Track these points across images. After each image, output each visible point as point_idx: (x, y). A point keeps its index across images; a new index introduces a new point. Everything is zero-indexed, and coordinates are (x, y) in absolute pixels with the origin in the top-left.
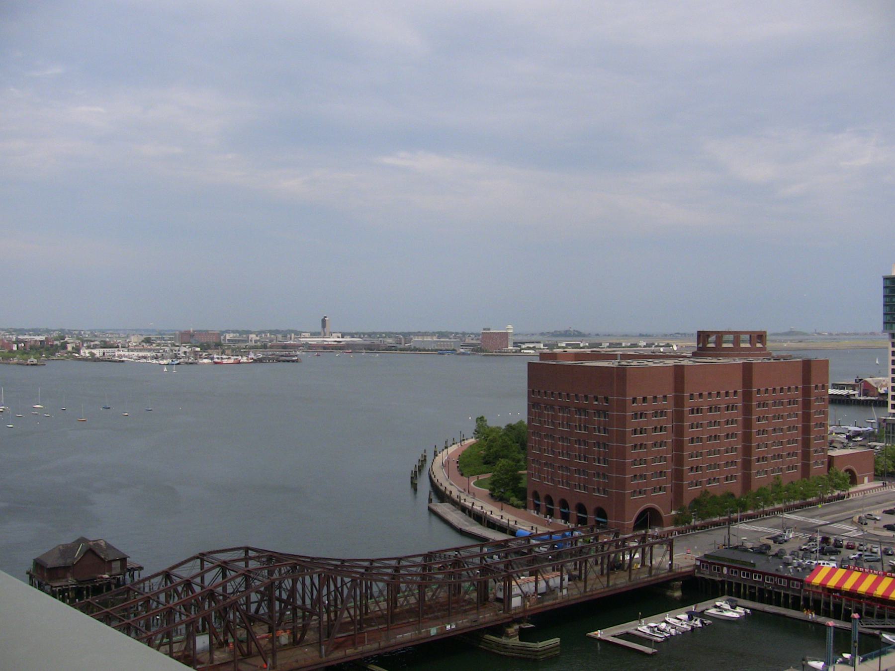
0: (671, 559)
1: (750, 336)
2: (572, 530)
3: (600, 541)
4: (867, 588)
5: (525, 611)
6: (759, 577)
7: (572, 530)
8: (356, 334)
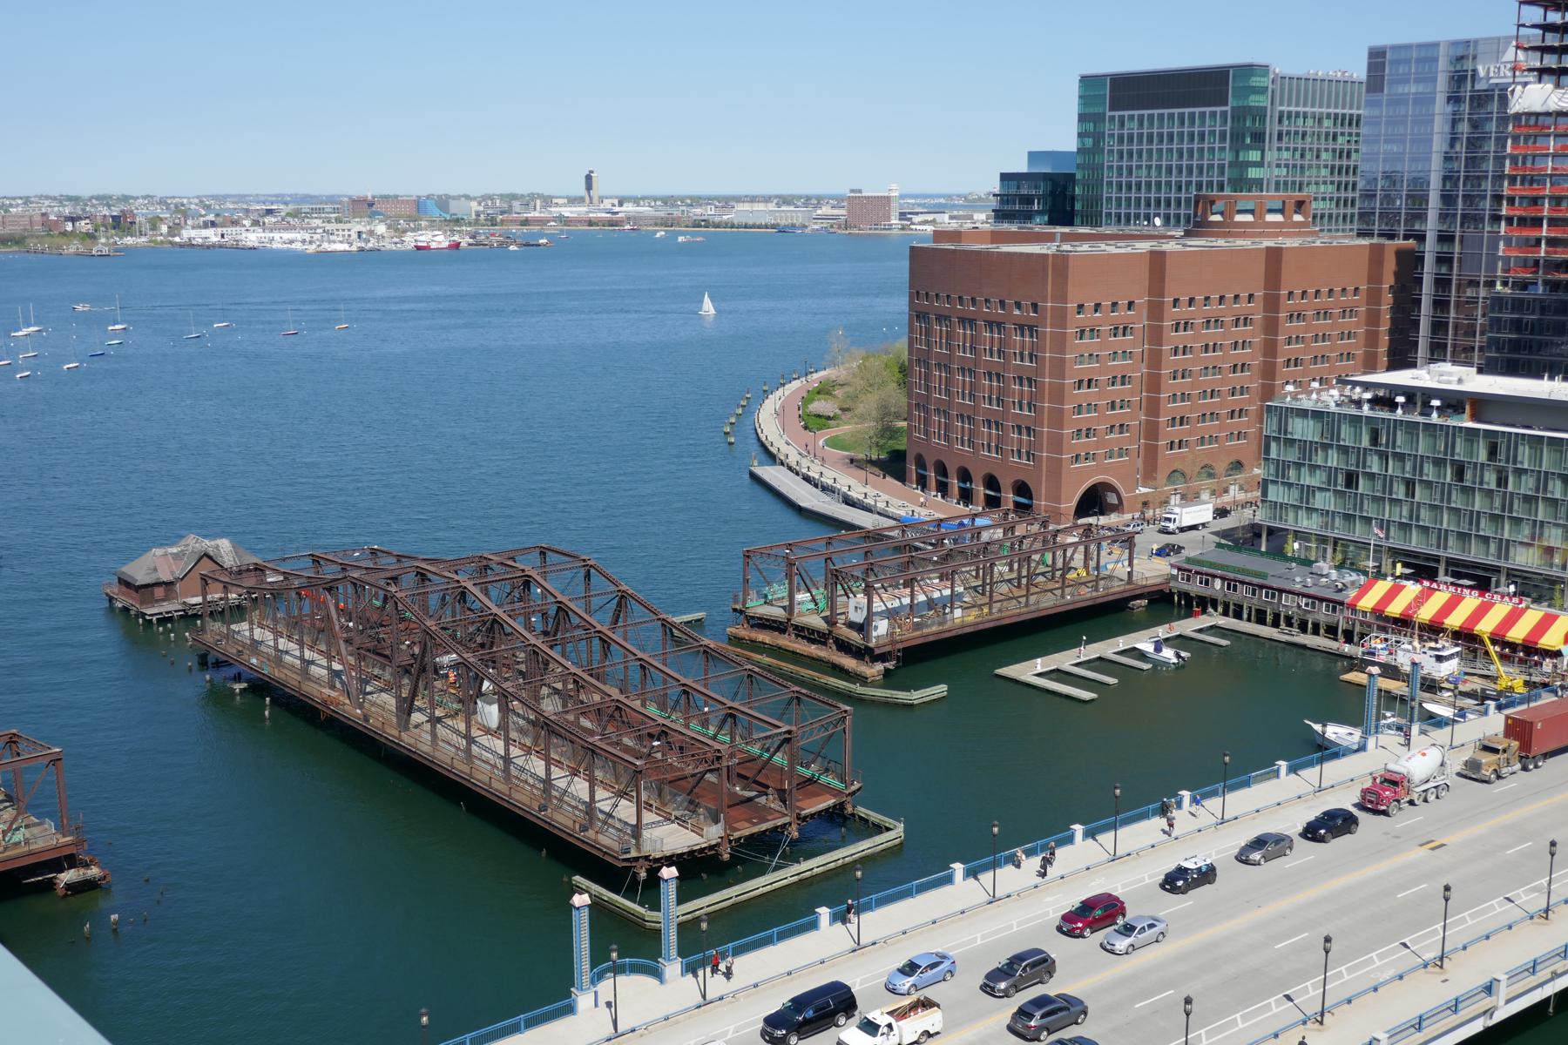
0: (1131, 564)
1: (1284, 202)
2: (974, 517)
3: (1017, 534)
4: (1434, 612)
5: (893, 642)
6: (1273, 596)
7: (974, 517)
8: (644, 198)
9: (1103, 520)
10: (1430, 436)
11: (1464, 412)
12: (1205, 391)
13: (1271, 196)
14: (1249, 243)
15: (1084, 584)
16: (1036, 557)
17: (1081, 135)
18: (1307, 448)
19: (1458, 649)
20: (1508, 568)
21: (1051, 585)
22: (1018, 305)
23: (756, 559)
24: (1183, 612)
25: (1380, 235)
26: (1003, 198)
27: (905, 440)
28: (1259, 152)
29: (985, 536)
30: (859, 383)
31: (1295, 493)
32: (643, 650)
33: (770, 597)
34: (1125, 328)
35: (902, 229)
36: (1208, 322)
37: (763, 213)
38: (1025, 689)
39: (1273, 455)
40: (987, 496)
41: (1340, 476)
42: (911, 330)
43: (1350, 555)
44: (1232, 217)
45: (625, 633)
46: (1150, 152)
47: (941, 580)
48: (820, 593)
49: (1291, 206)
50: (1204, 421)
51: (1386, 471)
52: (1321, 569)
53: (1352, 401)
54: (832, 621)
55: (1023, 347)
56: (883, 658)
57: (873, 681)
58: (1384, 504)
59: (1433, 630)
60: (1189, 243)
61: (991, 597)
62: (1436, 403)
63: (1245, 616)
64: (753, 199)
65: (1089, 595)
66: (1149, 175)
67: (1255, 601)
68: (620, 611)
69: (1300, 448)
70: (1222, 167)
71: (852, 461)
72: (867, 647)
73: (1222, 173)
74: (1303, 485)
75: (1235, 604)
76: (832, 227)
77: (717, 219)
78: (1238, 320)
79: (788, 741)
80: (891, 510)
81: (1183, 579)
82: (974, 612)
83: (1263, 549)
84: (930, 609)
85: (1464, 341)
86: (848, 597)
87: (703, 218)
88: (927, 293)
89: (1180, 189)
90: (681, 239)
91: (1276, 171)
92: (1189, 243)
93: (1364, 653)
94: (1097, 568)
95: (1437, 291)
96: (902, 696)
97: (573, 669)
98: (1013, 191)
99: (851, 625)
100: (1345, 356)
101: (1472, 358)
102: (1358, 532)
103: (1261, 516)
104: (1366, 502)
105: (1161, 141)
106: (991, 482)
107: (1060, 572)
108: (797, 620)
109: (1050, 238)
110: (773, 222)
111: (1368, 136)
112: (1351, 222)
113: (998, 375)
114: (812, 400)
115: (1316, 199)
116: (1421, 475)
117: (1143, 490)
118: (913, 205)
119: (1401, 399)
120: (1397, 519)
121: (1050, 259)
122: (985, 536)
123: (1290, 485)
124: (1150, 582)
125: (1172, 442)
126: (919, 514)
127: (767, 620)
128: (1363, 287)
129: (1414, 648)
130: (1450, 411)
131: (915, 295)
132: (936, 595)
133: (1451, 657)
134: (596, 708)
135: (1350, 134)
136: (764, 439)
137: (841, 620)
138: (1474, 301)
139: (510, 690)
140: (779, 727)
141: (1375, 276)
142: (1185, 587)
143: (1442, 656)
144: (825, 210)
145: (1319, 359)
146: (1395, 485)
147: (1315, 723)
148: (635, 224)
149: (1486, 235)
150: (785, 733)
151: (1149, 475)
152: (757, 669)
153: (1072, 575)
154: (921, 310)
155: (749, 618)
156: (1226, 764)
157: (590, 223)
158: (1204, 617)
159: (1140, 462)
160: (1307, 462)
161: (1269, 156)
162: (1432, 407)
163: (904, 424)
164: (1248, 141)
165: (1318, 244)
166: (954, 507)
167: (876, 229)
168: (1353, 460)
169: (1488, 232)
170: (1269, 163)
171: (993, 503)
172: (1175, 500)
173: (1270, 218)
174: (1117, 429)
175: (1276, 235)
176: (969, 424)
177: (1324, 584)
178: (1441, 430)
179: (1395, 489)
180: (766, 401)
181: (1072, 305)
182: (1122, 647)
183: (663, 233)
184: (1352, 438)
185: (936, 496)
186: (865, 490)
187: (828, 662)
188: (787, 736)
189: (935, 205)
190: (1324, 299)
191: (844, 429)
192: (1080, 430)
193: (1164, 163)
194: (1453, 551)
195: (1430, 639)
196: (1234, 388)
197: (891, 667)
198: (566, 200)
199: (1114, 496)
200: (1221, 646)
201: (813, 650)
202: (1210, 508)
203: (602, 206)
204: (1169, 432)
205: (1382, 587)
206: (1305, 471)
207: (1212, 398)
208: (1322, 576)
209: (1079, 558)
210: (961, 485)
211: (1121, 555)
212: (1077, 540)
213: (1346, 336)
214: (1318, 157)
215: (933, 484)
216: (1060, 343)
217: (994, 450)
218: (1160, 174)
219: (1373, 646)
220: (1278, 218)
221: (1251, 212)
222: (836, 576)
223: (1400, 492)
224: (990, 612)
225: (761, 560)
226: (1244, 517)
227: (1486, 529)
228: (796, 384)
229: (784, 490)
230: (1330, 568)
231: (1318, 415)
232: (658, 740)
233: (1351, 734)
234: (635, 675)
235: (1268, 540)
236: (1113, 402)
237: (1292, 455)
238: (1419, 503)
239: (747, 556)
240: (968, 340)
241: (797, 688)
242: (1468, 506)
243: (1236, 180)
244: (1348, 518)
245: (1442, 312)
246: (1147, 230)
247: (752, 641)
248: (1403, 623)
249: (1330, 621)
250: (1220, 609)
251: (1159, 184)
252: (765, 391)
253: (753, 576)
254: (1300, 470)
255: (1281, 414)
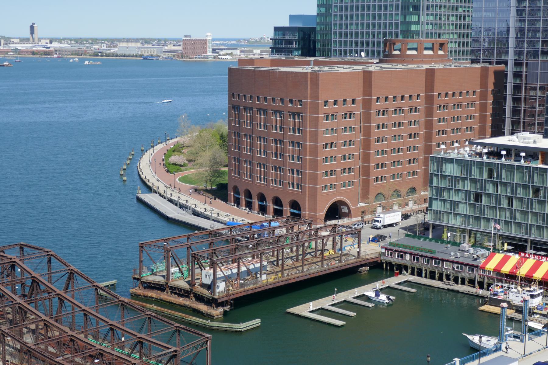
1: (433, 44)
3: (295, 231)
4: (544, 274)
5: (228, 295)
8: (64, 39)
9: (341, 222)
10: (520, 172)
11: (538, 159)
12: (394, 149)
13: (427, 41)
14: (416, 66)
15: (333, 258)
16: (306, 244)
17: (319, 6)
18: (453, 180)
19: (542, 291)
20: (531, 240)
21: (315, 260)
22: (291, 101)
23: (147, 248)
24: (388, 273)
25: (483, 62)
26: (275, 40)
27: (227, 178)
28: (417, 16)
29: (277, 232)
30: (198, 145)
31: (448, 205)
32: (86, 305)
33: (155, 270)
34: (350, 114)
35: (214, 58)
36: (396, 110)
37: (133, 48)
38: (297, 318)
39: (435, 184)
40: (275, 210)
41: (472, 196)
42: (230, 115)
43: (478, 239)
44: (405, 52)
45: (73, 295)
46: (357, 16)
47: (253, 258)
48: (184, 267)
49: (437, 46)
50: (394, 166)
51: (497, 192)
52: (465, 247)
53: (477, 154)
54: (191, 283)
55: (294, 125)
56: (223, 304)
57: (217, 318)
58: (528, 216)
59: (528, 280)
60: (383, 66)
61: (283, 267)
62: (523, 154)
63: (424, 275)
64: (128, 40)
65: (337, 265)
66: (357, 29)
67: (429, 266)
68: (69, 282)
69: (449, 180)
70: (397, 24)
71: (196, 190)
72: (213, 299)
73: (397, 27)
74: (451, 201)
75: (417, 269)
76: (174, 56)
77: (108, 52)
78: (411, 109)
79: (175, 356)
80: (221, 218)
81: (388, 255)
82: (273, 276)
83: (430, 237)
84: (248, 275)
85: (529, 120)
86: (202, 270)
87: (99, 51)
88: (239, 95)
89: (374, 36)
90: (86, 62)
91: (426, 27)
92: (383, 66)
93: (491, 295)
94: (341, 249)
95: (514, 93)
96: (235, 326)
97: (44, 317)
98: (281, 37)
99: (203, 286)
100: (469, 129)
101: (534, 129)
102: (483, 227)
103: (429, 218)
104: (486, 210)
105: (363, 10)
106: (277, 201)
107: (320, 252)
108: (171, 283)
109: (308, 63)
110: (140, 53)
111: (476, 8)
112: (467, 55)
113: (280, 141)
114: (171, 156)
115: (451, 42)
116: (516, 194)
117: (362, 205)
118: (220, 44)
119: (504, 152)
120: (504, 219)
121: (309, 76)
122: (277, 232)
123: (445, 201)
124: (370, 257)
125: (377, 178)
126: (237, 220)
127: (154, 284)
128: (478, 91)
129: (519, 291)
130: (530, 158)
131: (232, 95)
132: (252, 267)
133: (538, 295)
134: (57, 341)
135: (465, 7)
136: (144, 178)
137: (198, 282)
138: (534, 98)
139: (7, 331)
140: (169, 348)
141: (484, 85)
142: (389, 259)
143: (534, 295)
144: (170, 47)
145: (455, 131)
146: (502, 200)
147: (469, 334)
148: (59, 54)
149: (540, 62)
150: (173, 352)
151: (365, 196)
152: (153, 314)
153: (326, 254)
154: (261, 107)
155: (143, 283)
156: (428, 362)
157: (33, 53)
158: (400, 276)
159: (360, 189)
160: (454, 188)
161: (422, 19)
162: (521, 156)
163: (226, 169)
164: (411, 10)
165: (453, 67)
166: (255, 217)
167: (199, 58)
168: (479, 186)
169: (541, 61)
170: (422, 22)
171: (278, 213)
172: (379, 210)
173: (426, 52)
174: (347, 170)
175: (430, 62)
176: (264, 168)
177: (466, 256)
178: (526, 169)
179: (502, 202)
180: (144, 156)
181: (321, 101)
182: (357, 295)
183: (77, 59)
184: (478, 174)
185: (246, 209)
186: (205, 207)
187: (190, 308)
188: (174, 353)
189: (231, 45)
190: (457, 97)
191: (191, 172)
192: (327, 172)
193: (365, 22)
194: (534, 236)
195: (527, 286)
196: (410, 147)
197: (228, 310)
198: (18, 40)
199: (346, 208)
200: (412, 292)
201: (182, 301)
202: (399, 214)
203: (40, 44)
204: (375, 172)
205: (498, 257)
206: (452, 193)
207: (398, 152)
208: (465, 251)
209: (330, 244)
210: (260, 203)
211: (354, 241)
212: (328, 233)
213: (469, 117)
214: (448, 19)
215: (244, 203)
216: (315, 122)
217: (278, 183)
218: (363, 28)
219: (496, 290)
220: (430, 52)
221: (416, 49)
222: (194, 257)
223: (504, 203)
224: (282, 276)
225: (150, 249)
226: (419, 218)
227: (519, 218)
228: (160, 146)
229: (157, 207)
230: (469, 247)
231: (458, 162)
232: (98, 359)
233: (489, 340)
234: (80, 319)
235: (432, 232)
236: (345, 156)
237: (445, 184)
238: (515, 210)
239: (142, 246)
240: (263, 121)
241: (178, 325)
242: (542, 211)
243: (405, 31)
244: (477, 218)
245: (518, 104)
246: (357, 59)
247: (145, 296)
248: (511, 277)
249: (471, 276)
250: (409, 271)
251: (362, 34)
252: (142, 150)
253: (145, 257)
254: (450, 192)
255: (439, 161)
